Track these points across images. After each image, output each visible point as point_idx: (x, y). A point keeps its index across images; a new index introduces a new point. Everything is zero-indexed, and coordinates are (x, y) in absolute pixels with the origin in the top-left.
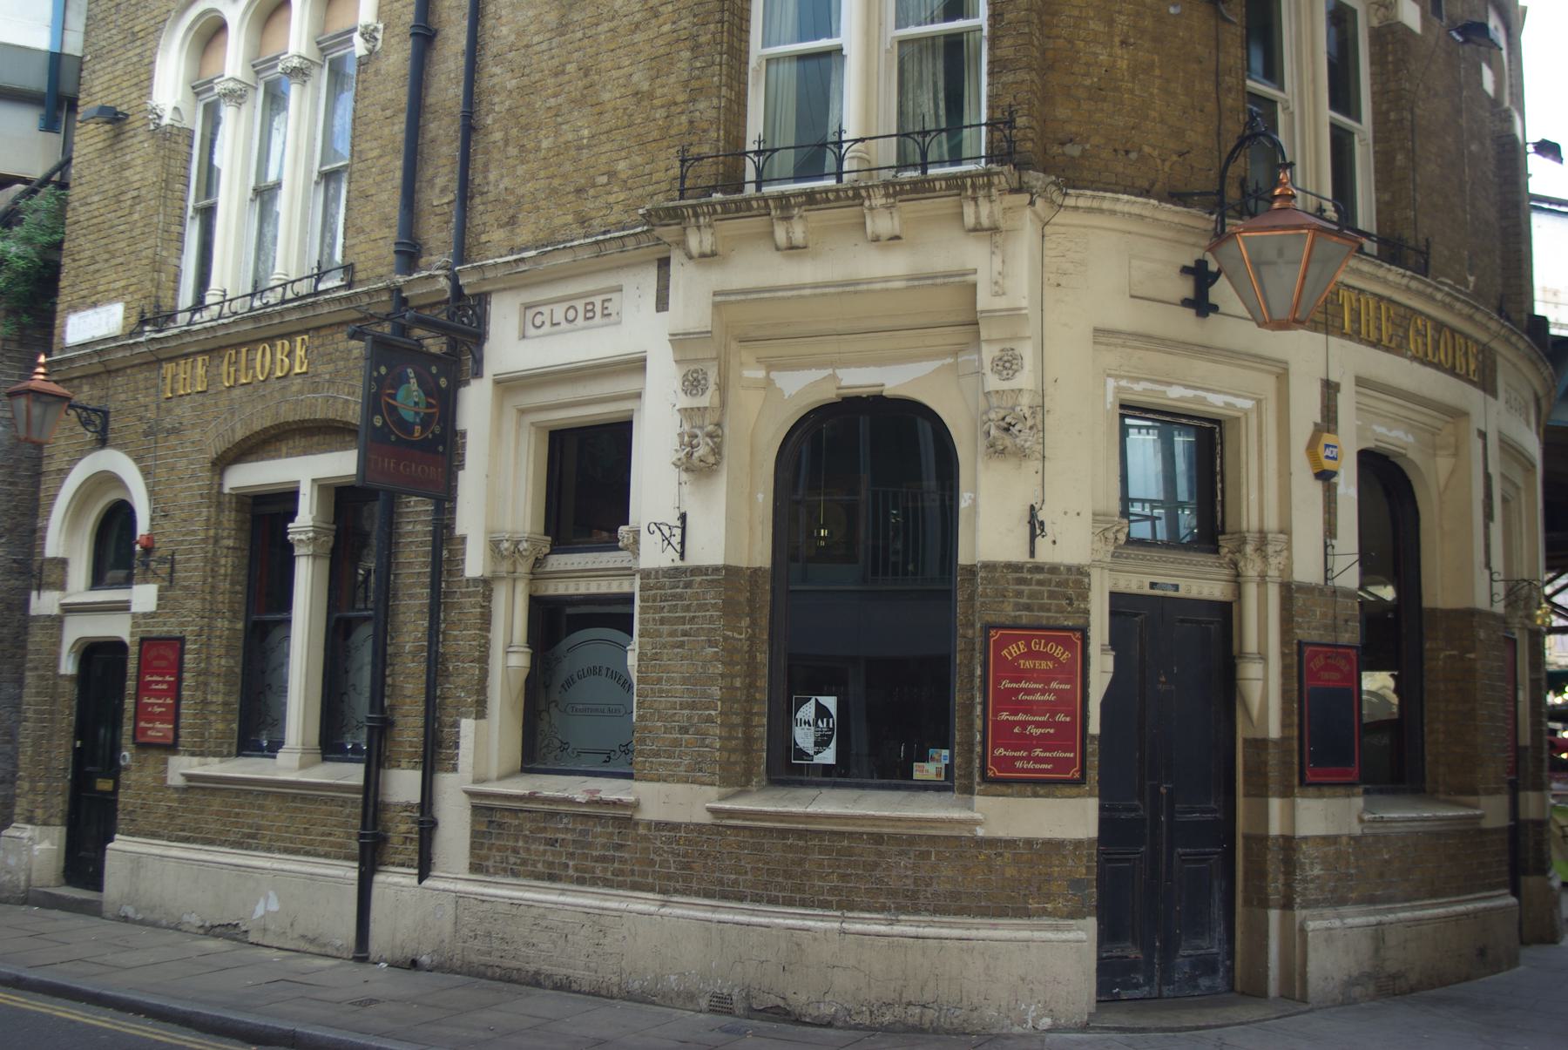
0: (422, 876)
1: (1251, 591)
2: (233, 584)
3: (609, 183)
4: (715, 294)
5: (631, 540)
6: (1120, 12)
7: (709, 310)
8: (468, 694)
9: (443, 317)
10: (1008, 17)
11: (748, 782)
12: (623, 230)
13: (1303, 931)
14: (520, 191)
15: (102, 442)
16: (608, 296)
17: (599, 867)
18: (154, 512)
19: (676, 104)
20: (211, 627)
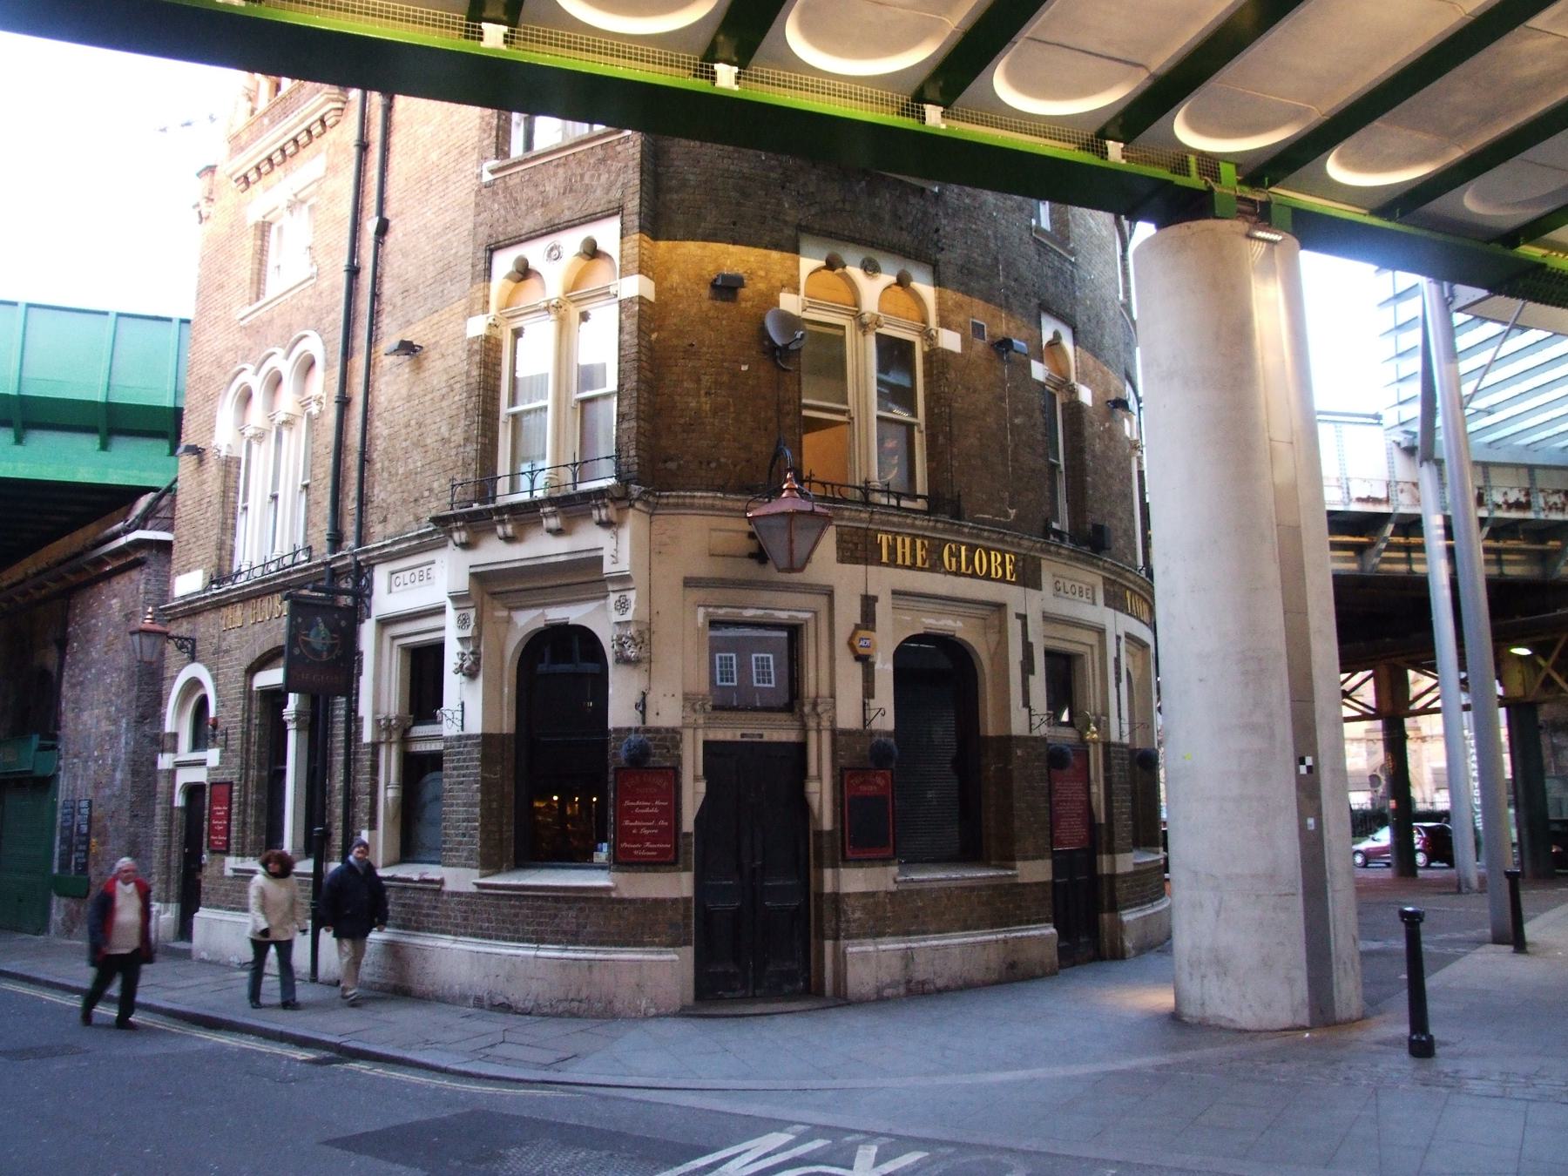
1: (813, 736)
6: (705, 374)
7: (467, 578)
10: (626, 386)
11: (501, 867)
13: (844, 953)
14: (389, 501)
15: (193, 659)
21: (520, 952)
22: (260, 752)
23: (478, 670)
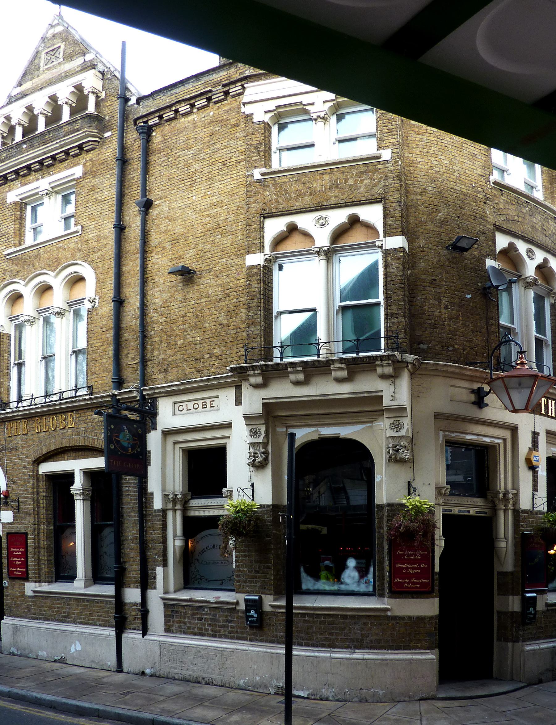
0: (144, 634)
2: (47, 510)
3: (210, 357)
4: (263, 399)
5: (229, 494)
8: (159, 556)
9: (137, 406)
12: (218, 375)
14: (170, 359)
16: (212, 399)
17: (222, 630)
18: (8, 481)
19: (240, 328)
20: (39, 529)
21: (317, 654)
22: (47, 514)
23: (267, 464)
